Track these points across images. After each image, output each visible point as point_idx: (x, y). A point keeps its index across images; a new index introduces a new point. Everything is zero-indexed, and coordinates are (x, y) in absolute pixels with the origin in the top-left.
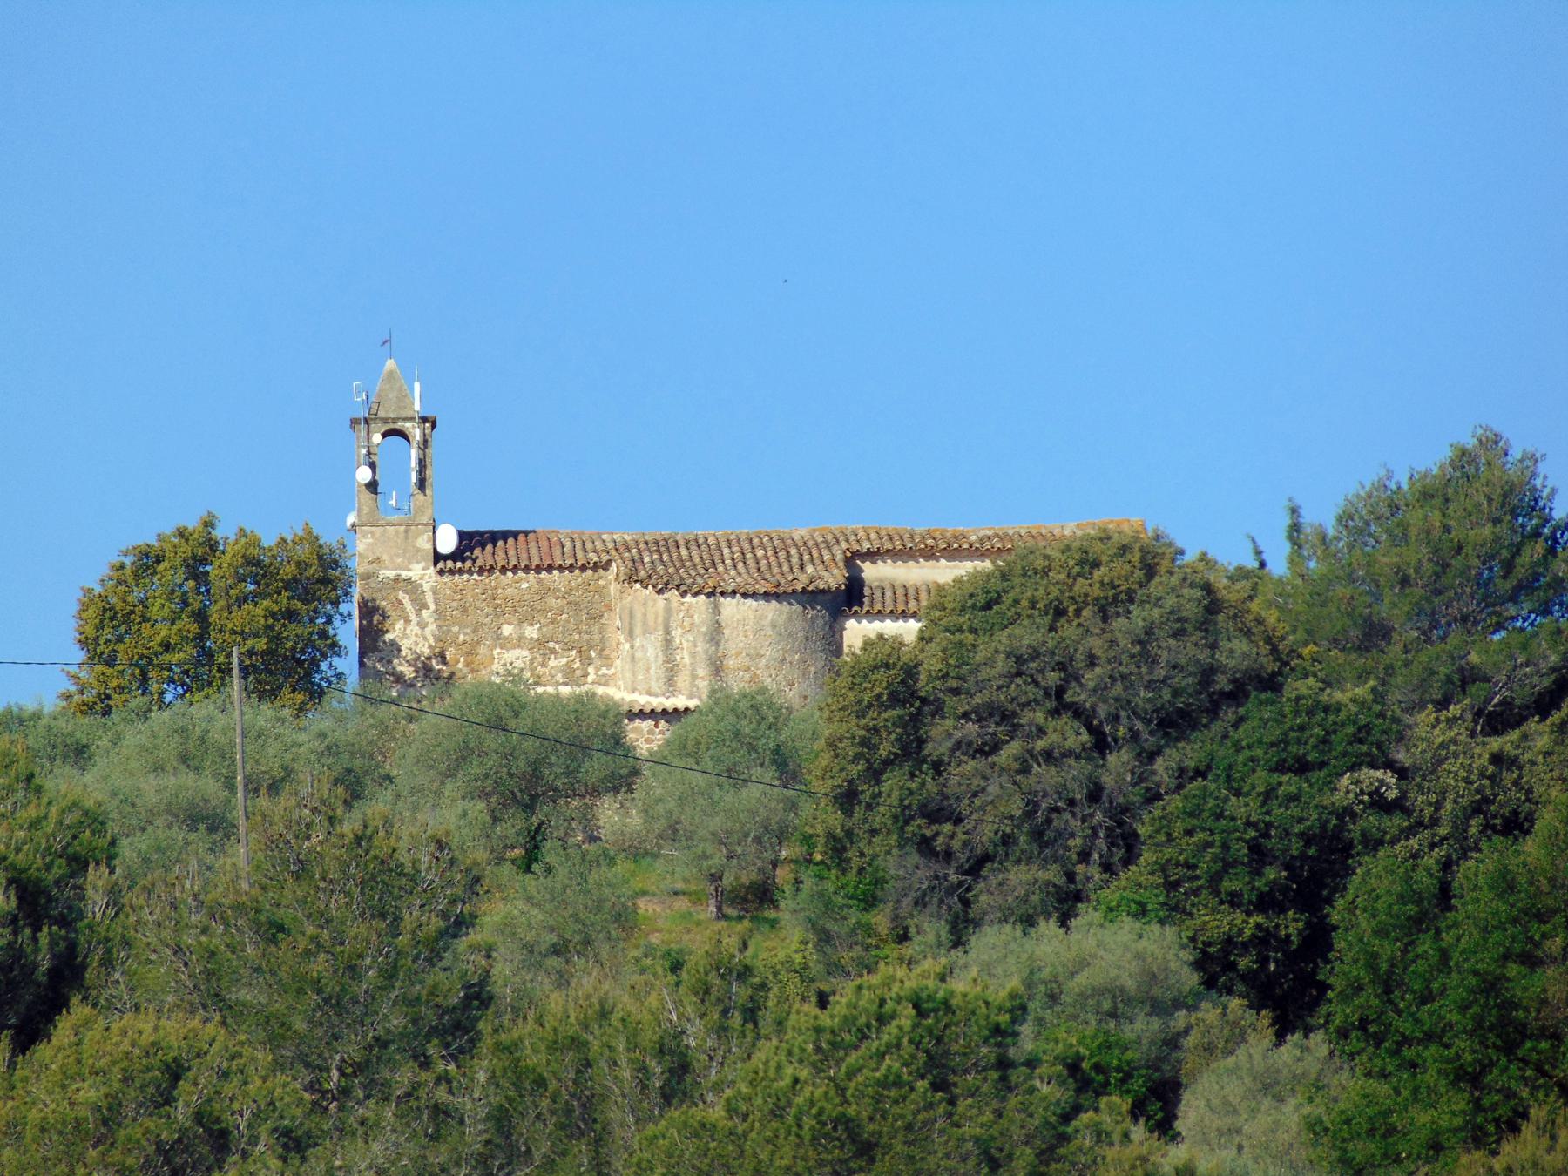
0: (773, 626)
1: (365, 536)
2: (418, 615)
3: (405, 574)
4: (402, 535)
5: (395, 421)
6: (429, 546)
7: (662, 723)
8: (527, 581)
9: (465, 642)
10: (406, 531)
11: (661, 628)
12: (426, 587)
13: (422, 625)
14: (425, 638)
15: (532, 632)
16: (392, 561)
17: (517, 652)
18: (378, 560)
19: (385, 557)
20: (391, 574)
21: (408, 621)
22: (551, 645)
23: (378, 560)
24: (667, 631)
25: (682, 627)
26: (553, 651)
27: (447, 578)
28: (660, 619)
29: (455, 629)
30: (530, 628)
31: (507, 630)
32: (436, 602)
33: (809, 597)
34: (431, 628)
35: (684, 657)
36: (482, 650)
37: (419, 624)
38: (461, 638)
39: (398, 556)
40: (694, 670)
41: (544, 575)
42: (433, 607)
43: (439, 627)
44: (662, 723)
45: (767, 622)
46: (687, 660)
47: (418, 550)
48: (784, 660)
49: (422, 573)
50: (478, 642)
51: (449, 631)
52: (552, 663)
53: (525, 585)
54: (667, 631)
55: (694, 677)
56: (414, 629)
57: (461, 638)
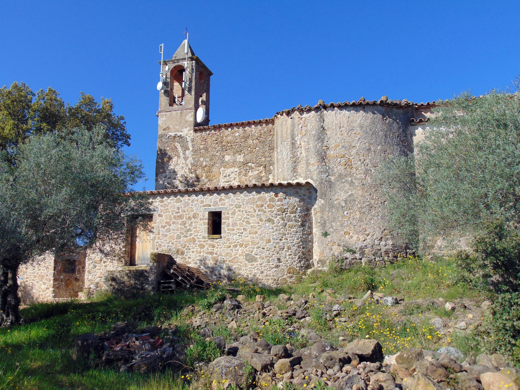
0: (361, 127)
1: (162, 117)
2: (184, 154)
3: (179, 134)
4: (179, 115)
5: (178, 60)
6: (192, 119)
7: (281, 194)
8: (239, 132)
9: (206, 166)
10: (181, 113)
11: (289, 137)
12: (189, 139)
13: (186, 159)
14: (187, 165)
15: (240, 158)
16: (174, 128)
17: (232, 169)
18: (168, 128)
19: (171, 126)
20: (172, 134)
21: (179, 157)
22: (250, 164)
23: (168, 128)
24: (293, 139)
25: (301, 134)
26: (251, 168)
27: (198, 134)
28: (289, 131)
29: (202, 159)
30: (239, 156)
31: (227, 158)
32: (193, 146)
33: (386, 108)
34: (190, 160)
35: (302, 153)
36: (214, 169)
37: (184, 158)
38: (204, 163)
39: (176, 125)
40: (308, 160)
41: (247, 128)
42: (191, 149)
43: (194, 158)
44: (281, 194)
45: (355, 124)
46: (304, 154)
47: (187, 121)
48: (369, 149)
49: (188, 132)
50: (213, 165)
51: (199, 160)
52: (250, 174)
53: (237, 134)
54: (293, 139)
55: (308, 164)
56: (181, 160)
57: (204, 163)
